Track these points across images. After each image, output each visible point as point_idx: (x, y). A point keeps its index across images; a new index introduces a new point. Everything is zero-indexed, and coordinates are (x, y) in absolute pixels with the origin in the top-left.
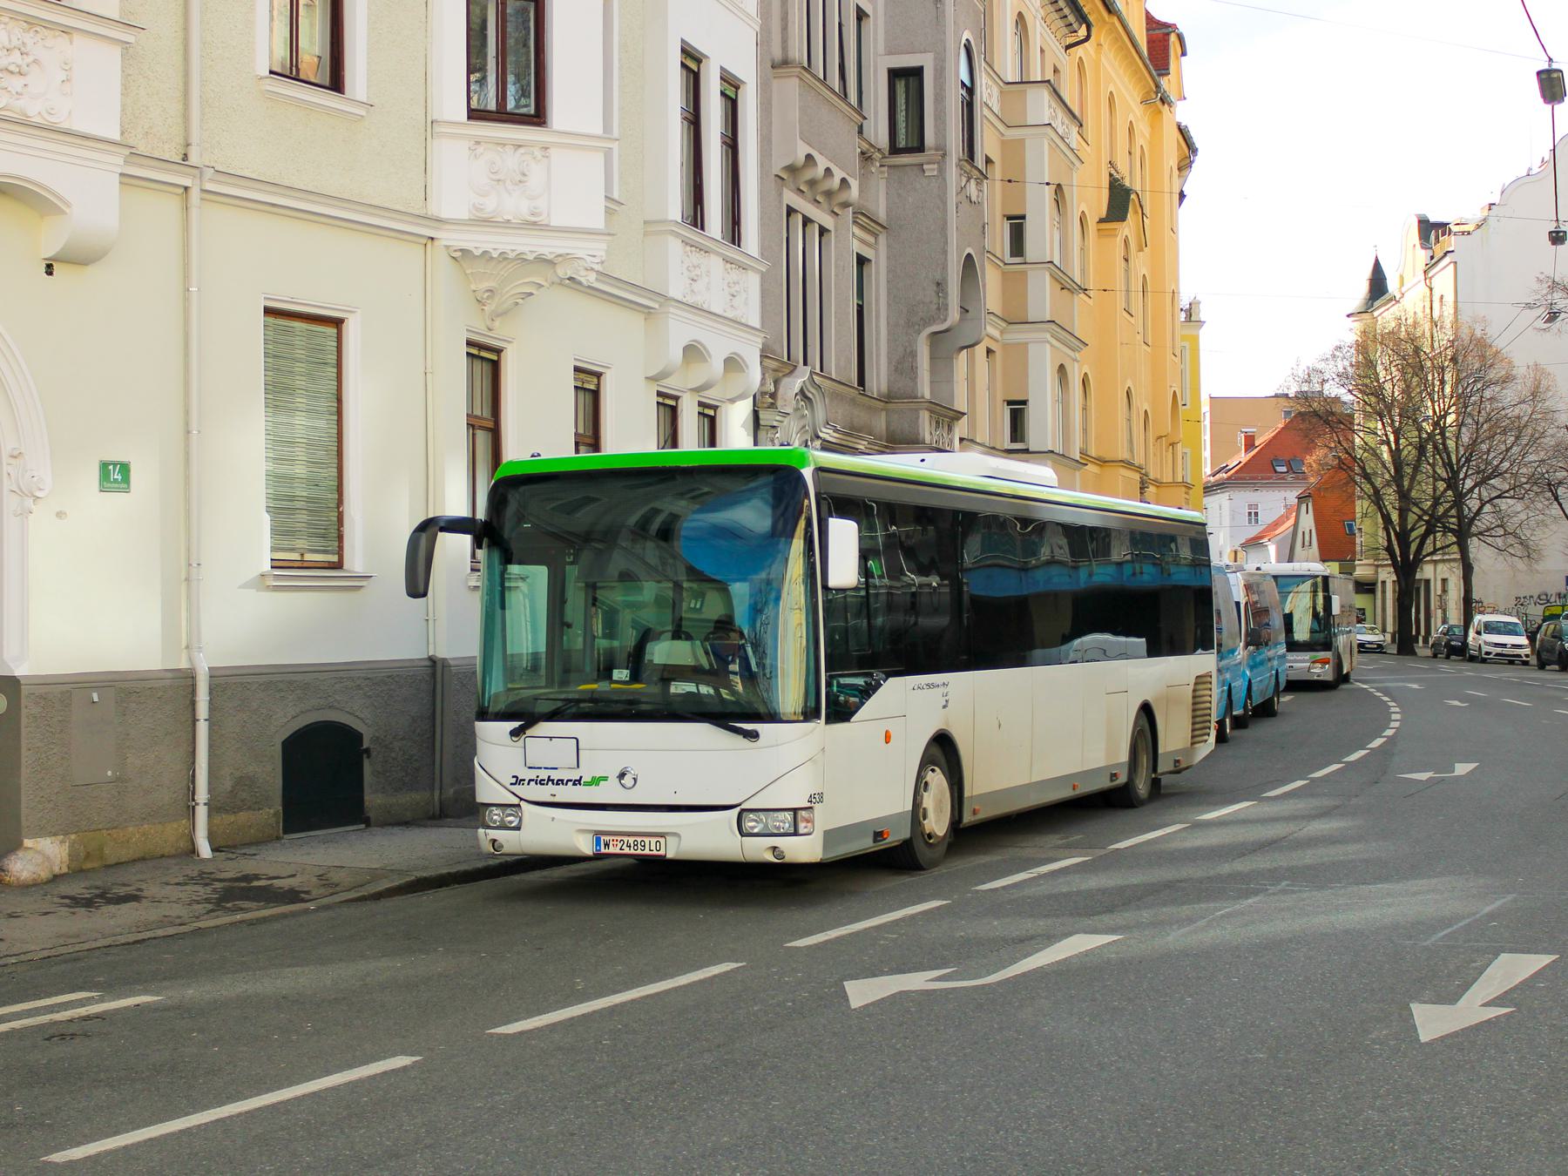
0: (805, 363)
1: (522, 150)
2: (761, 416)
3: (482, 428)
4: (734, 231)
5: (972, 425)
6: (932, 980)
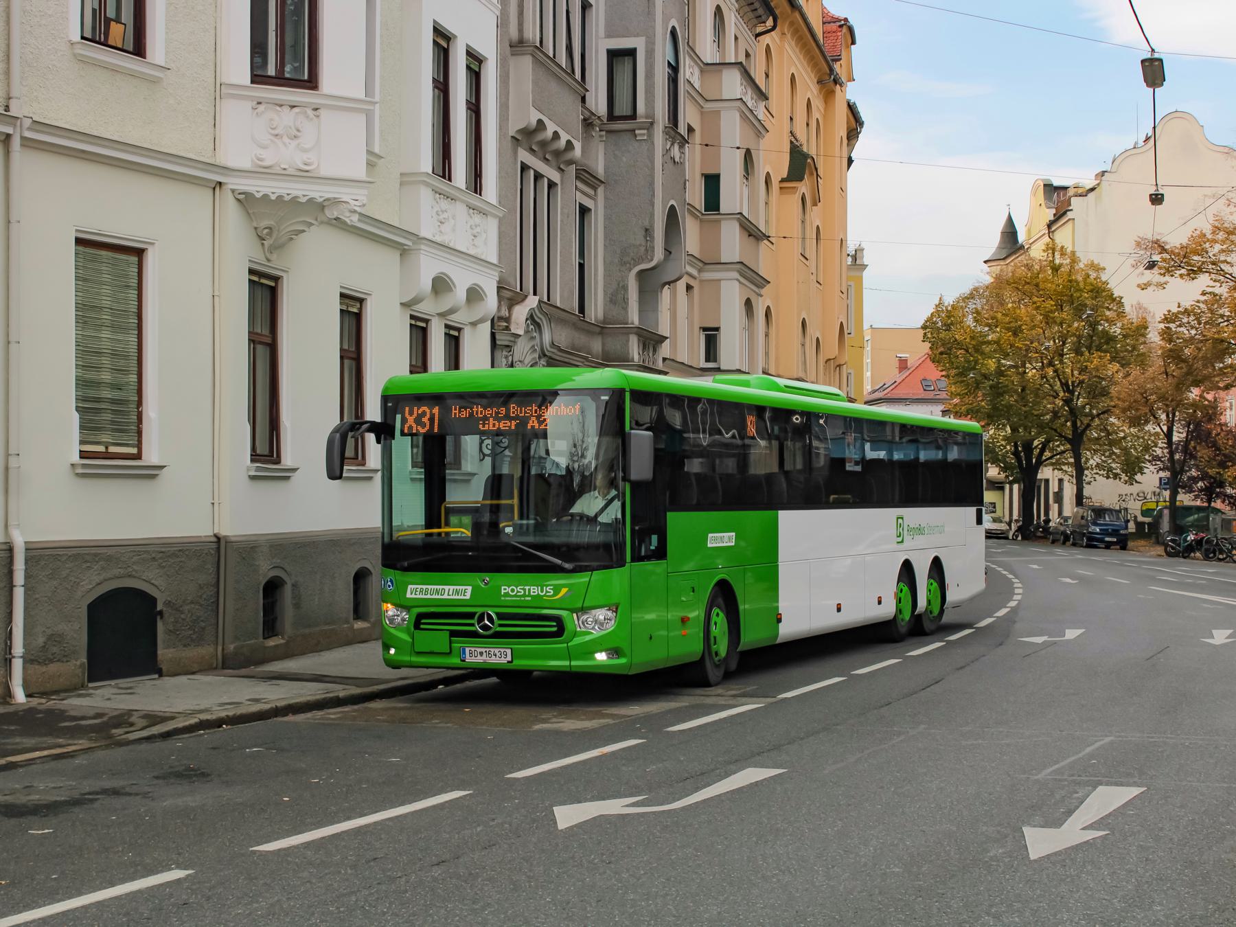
0: (535, 294)
1: (296, 110)
2: (497, 337)
3: (261, 343)
5: (674, 346)
6: (627, 806)
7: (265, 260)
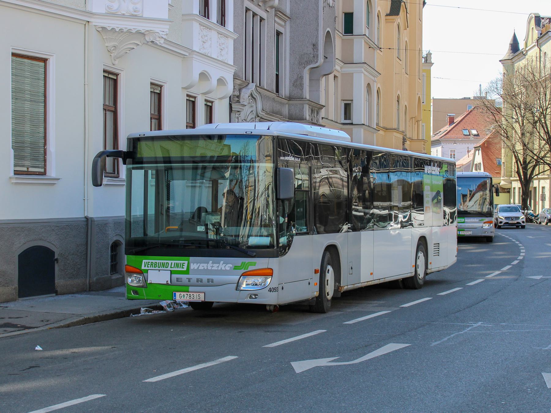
0: (253, 82)
2: (233, 106)
3: (109, 110)
4: (222, 21)
5: (327, 112)
6: (330, 362)
7: (112, 65)
